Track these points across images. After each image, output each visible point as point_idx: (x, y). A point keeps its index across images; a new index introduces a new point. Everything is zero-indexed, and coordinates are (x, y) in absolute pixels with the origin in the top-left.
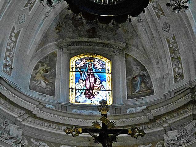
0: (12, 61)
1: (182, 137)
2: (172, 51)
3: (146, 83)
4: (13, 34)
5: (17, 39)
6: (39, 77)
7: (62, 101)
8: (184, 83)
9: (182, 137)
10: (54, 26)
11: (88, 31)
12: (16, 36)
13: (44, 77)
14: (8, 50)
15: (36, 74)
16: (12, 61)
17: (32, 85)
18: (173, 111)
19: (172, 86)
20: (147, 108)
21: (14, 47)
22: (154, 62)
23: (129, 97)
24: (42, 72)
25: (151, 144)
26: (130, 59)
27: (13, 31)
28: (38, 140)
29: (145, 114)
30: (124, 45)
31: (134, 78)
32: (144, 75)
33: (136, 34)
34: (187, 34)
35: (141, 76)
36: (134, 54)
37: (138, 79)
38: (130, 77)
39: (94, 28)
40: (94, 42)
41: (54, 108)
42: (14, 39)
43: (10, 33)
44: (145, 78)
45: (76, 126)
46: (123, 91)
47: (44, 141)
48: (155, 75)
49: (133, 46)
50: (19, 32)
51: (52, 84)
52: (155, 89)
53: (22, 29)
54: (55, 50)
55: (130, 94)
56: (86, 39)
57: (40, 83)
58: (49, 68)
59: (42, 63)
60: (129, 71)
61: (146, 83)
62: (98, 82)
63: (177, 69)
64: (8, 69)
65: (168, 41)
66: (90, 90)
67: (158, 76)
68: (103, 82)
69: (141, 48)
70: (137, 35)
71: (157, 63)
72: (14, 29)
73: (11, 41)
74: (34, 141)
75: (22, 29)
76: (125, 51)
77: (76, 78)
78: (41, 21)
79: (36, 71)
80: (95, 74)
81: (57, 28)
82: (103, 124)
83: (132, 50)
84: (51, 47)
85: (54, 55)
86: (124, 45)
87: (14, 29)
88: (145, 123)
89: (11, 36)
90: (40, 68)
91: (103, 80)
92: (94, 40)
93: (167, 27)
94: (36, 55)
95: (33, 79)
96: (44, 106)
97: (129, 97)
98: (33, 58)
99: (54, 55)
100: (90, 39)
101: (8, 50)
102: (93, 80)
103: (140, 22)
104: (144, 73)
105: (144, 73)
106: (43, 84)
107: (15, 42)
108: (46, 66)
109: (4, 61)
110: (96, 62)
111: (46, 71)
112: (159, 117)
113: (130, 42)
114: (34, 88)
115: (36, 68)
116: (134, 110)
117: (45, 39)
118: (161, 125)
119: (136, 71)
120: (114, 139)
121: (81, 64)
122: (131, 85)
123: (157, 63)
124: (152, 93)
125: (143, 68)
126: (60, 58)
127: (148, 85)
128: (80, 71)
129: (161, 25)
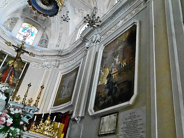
1: (49, 65)
2: (60, 37)
3: (46, 43)
5: (6, 5)
6: (8, 23)
7: (13, 35)
8: (58, 49)
9: (49, 65)
10: (22, 9)
11: (34, 17)
12: (6, 4)
15: (8, 21)
17: (4, 24)
18: (50, 56)
19: (54, 48)
20: (42, 51)
21: (3, 7)
22: (52, 38)
23: (38, 45)
24: (10, 22)
25: (38, 63)
26: (44, 33)
27: (5, 1)
29: (43, 52)
30: (45, 28)
31: (43, 40)
32: (47, 40)
33: (101, 71)
34: (67, 34)
35: (45, 40)
36: (47, 32)
37: (44, 41)
38: (42, 39)
39: (37, 17)
40: (35, 22)
41: (9, 36)
42: (4, 5)
43: (4, 1)
44: (46, 42)
45: (11, 44)
46: (37, 41)
48: (51, 42)
49: (48, 29)
50: (8, 3)
52: (48, 46)
53: (9, 3)
54: (19, 17)
55: (39, 44)
56: (33, 19)
57: (8, 25)
60: (42, 37)
61: (46, 43)
62: (30, 35)
63: (58, 43)
65: (60, 33)
66: (25, 37)
67: (51, 43)
69: (50, 31)
70: (51, 27)
71: (53, 39)
72: (6, 1)
73: (2, 5)
75: (9, 3)
76: (44, 30)
77: (23, 30)
78: (18, 4)
79: (8, 20)
81: (23, 10)
82: (21, 47)
83: (47, 31)
84: (18, 15)
85: (18, 18)
86: (45, 28)
88: (39, 56)
89: (3, 3)
90: (10, 20)
92: (36, 21)
93: (61, 29)
95: (5, 22)
96: (5, 33)
97: (38, 45)
98: (9, 15)
99: (18, 18)
100: (34, 20)
102: (28, 34)
103: (53, 23)
104: (47, 40)
105: (47, 40)
106: (9, 26)
107: (4, 6)
108: (13, 20)
112: (44, 55)
113: (47, 28)
114: (4, 26)
115: (9, 19)
116: (38, 50)
117: (17, 11)
118: (44, 58)
119: (45, 38)
120: (23, 53)
121: (27, 27)
122: (41, 42)
123: (53, 39)
124: (47, 47)
125: (48, 38)
126: (20, 21)
127: (47, 44)
128: (25, 29)
129: (60, 27)
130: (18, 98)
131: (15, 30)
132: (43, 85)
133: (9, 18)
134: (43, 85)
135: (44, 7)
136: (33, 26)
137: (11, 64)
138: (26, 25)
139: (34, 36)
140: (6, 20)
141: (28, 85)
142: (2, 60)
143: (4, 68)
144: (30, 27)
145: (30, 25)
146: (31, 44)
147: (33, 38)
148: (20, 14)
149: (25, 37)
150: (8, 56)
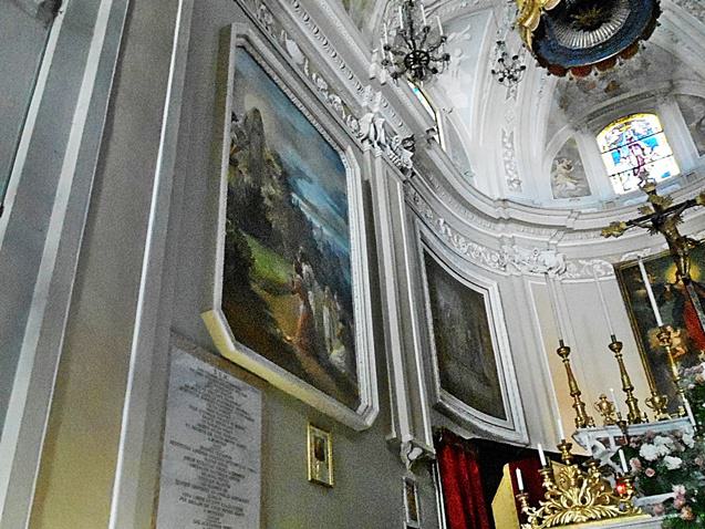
0: (516, 173)
4: (505, 140)
6: (561, 179)
11: (607, 90)
13: (568, 176)
14: (506, 162)
16: (516, 173)
17: (556, 192)
26: (683, 99)
28: (588, 259)
30: (666, 85)
38: (694, 124)
42: (509, 145)
47: (600, 257)
49: (681, 79)
50: (512, 133)
51: (583, 179)
58: (674, 463)
59: (560, 160)
62: (647, 150)
64: (515, 185)
66: (638, 168)
68: (655, 148)
72: (504, 133)
74: (584, 262)
79: (554, 174)
80: (639, 142)
82: (654, 205)
85: (572, 141)
87: (504, 133)
89: (504, 143)
90: (559, 166)
91: (653, 146)
94: (547, 153)
98: (544, 160)
99: (572, 141)
101: (506, 162)
102: (639, 152)
106: (571, 186)
109: (507, 177)
110: (634, 125)
111: (569, 167)
115: (554, 168)
120: (677, 218)
126: (584, 144)
128: (616, 148)
130: (604, 405)
131: (593, 178)
132: (613, 337)
133: (551, 165)
134: (613, 337)
135: (604, 32)
136: (630, 120)
137: (678, 280)
138: (608, 136)
139: (661, 138)
140: (548, 177)
141: (611, 347)
142: (642, 291)
143: (670, 304)
144: (624, 128)
145: (617, 125)
146: (675, 171)
147: (663, 148)
148: (567, 126)
149: (638, 168)
150: (644, 264)
